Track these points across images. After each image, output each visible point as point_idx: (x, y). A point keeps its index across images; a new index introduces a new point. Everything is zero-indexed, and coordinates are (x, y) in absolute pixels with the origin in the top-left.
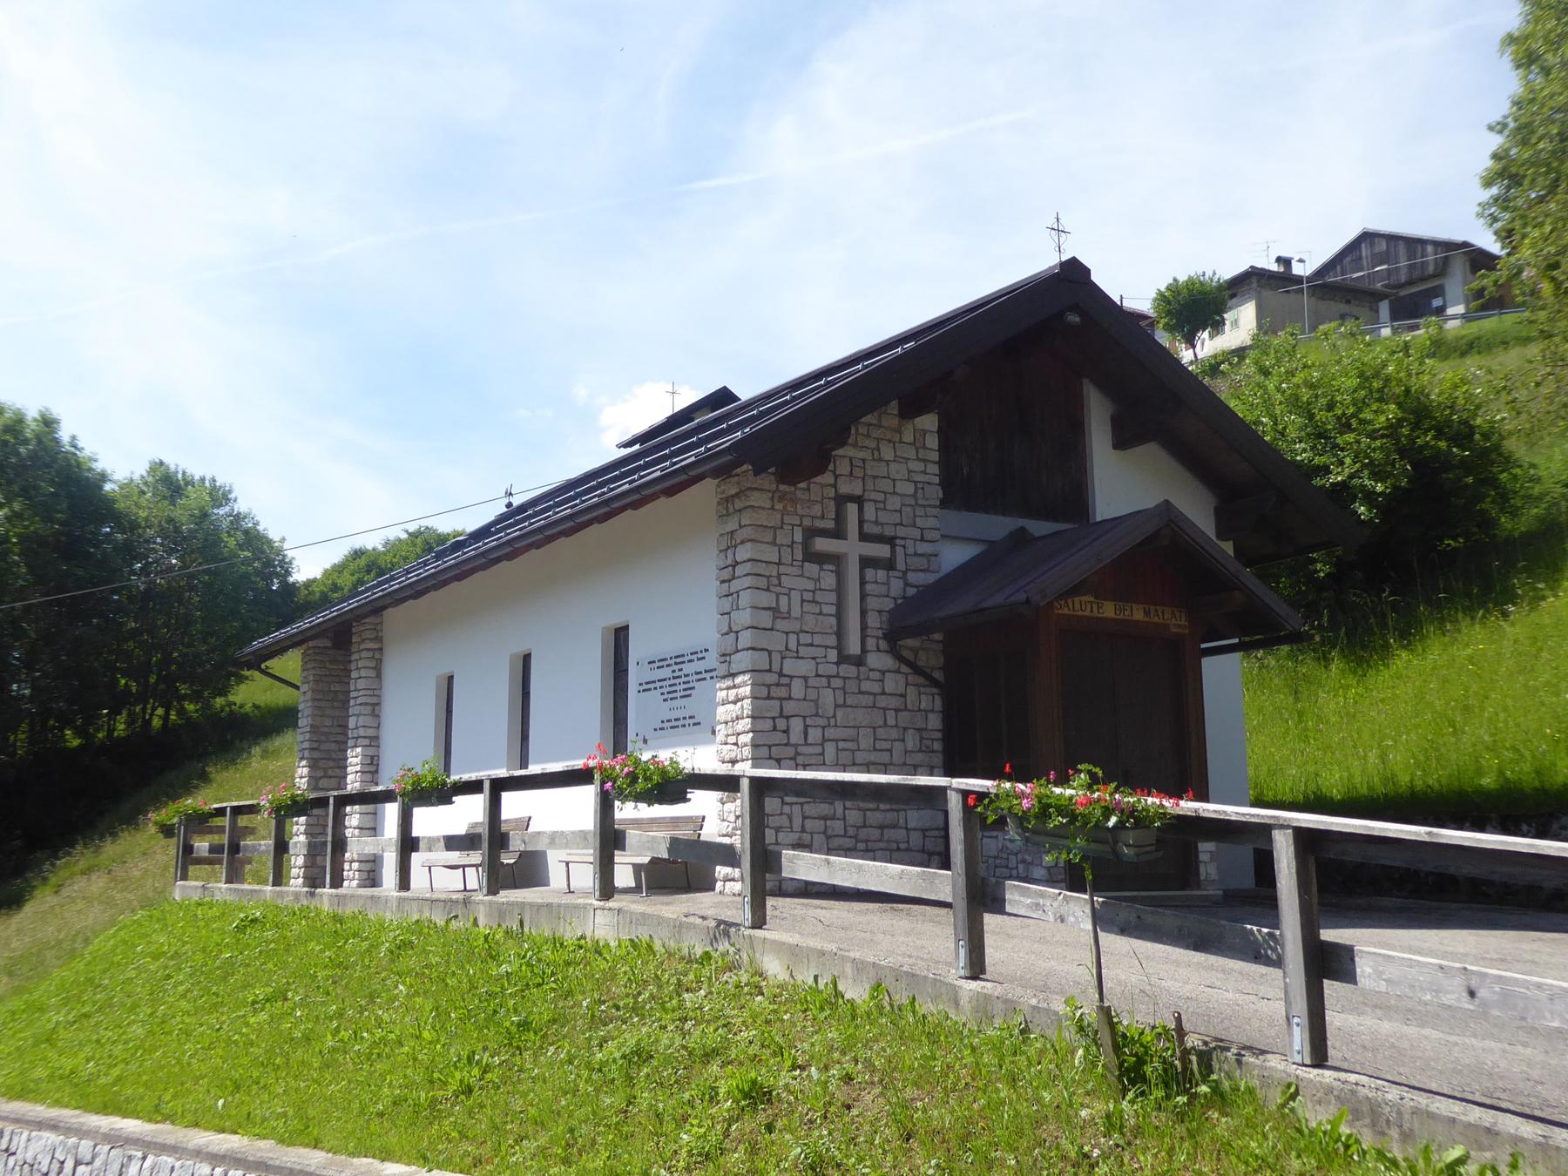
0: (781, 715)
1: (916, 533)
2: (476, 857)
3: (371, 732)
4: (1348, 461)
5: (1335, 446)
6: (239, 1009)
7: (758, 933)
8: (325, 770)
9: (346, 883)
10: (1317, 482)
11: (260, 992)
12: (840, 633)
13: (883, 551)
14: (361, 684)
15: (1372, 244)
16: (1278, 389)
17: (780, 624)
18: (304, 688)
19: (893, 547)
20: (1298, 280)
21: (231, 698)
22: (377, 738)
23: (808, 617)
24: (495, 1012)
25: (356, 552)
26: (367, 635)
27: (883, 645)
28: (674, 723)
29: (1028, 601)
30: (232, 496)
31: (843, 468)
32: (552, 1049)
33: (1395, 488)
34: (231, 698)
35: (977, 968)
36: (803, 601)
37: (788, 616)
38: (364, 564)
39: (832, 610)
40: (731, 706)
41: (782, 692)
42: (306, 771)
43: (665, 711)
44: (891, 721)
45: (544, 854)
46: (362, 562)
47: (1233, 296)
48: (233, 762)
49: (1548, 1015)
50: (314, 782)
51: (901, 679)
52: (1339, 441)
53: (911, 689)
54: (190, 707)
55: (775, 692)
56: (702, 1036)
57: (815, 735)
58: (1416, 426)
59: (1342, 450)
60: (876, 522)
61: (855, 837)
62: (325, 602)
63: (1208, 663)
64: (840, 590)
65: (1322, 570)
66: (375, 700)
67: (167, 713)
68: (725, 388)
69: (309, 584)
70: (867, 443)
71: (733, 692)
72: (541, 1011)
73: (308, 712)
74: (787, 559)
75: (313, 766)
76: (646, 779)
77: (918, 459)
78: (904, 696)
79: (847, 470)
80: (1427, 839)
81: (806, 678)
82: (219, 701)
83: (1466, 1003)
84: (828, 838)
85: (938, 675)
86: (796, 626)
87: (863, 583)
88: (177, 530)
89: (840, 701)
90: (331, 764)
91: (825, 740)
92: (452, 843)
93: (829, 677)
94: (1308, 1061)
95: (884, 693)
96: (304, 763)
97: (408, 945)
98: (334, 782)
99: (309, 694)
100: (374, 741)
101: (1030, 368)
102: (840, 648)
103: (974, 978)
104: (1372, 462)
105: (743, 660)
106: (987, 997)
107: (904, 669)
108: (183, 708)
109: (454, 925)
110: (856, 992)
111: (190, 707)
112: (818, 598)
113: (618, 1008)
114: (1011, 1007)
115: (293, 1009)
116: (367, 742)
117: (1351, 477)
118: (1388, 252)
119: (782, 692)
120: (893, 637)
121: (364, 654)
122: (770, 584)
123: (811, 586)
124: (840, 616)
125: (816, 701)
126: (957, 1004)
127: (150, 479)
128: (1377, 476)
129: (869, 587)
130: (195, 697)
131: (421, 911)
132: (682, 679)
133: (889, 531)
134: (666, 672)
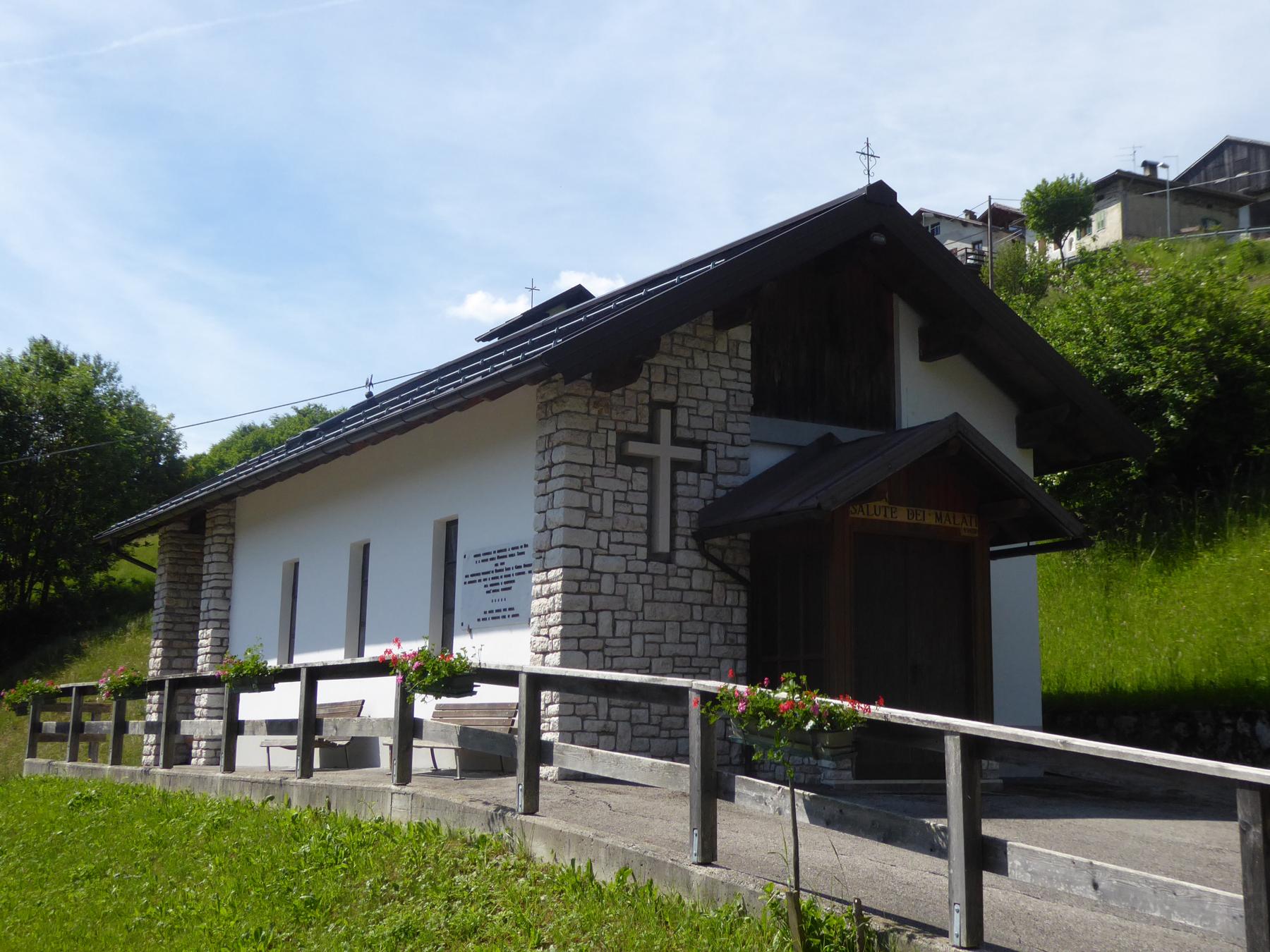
0: (591, 610)
1: (727, 438)
2: (292, 739)
3: (221, 615)
4: (1159, 371)
5: (1149, 357)
6: (60, 884)
7: (530, 819)
8: (179, 650)
9: (193, 761)
10: (1130, 391)
11: (82, 868)
12: (650, 532)
13: (693, 454)
14: (213, 568)
15: (1234, 153)
16: (1098, 301)
17: (592, 523)
18: (161, 571)
19: (704, 451)
20: (1162, 184)
21: (111, 573)
22: (227, 620)
23: (619, 517)
24: (289, 890)
25: (245, 429)
26: (219, 521)
27: (692, 543)
28: (495, 614)
29: (819, 506)
30: (117, 375)
31: (658, 376)
32: (332, 926)
33: (1201, 397)
34: (111, 573)
35: (708, 856)
36: (615, 501)
37: (600, 515)
38: (251, 440)
39: (644, 510)
40: (543, 600)
41: (593, 587)
42: (160, 651)
43: (488, 602)
44: (697, 616)
45: (376, 739)
46: (250, 439)
47: (1100, 198)
48: (108, 637)
49: (1152, 906)
50: (167, 666)
51: (708, 576)
52: (1152, 352)
53: (717, 586)
54: (69, 582)
55: (586, 587)
56: (467, 914)
57: (622, 628)
58: (1225, 340)
59: (1155, 360)
60: (689, 428)
61: (659, 725)
62: (211, 475)
63: (997, 566)
64: (652, 492)
65: (1135, 472)
66: (225, 584)
67: (46, 587)
68: (580, 286)
69: (196, 459)
70: (682, 352)
71: (546, 586)
72: (329, 891)
73: (163, 594)
74: (600, 460)
75: (167, 646)
76: (435, 673)
77: (731, 368)
78: (711, 592)
79: (661, 378)
80: (1061, 748)
81: (615, 575)
82: (98, 576)
83: (1091, 895)
84: (632, 725)
85: (745, 573)
86: (607, 524)
87: (674, 484)
88: (59, 408)
89: (648, 596)
90: (185, 644)
91: (632, 633)
92: (275, 727)
93: (638, 574)
94: (964, 944)
95: (691, 589)
96: (158, 642)
97: (224, 824)
98: (187, 662)
99: (165, 577)
100: (224, 624)
101: (845, 281)
102: (650, 545)
103: (705, 863)
104: (1181, 374)
105: (556, 555)
106: (714, 882)
107: (711, 566)
108: (63, 584)
109: (272, 805)
110: (606, 876)
111: (69, 582)
112: (630, 499)
113: (397, 888)
114: (732, 890)
115: (110, 886)
116: (217, 624)
117: (1163, 386)
118: (1248, 160)
119: (593, 587)
120: (701, 537)
121: (216, 539)
122: (584, 485)
123: (623, 487)
124: (651, 516)
125: (625, 597)
126: (689, 887)
127: (33, 357)
128: (1187, 386)
129: (680, 489)
130: (76, 572)
131: (242, 792)
132: (503, 573)
133: (701, 436)
134: (489, 566)
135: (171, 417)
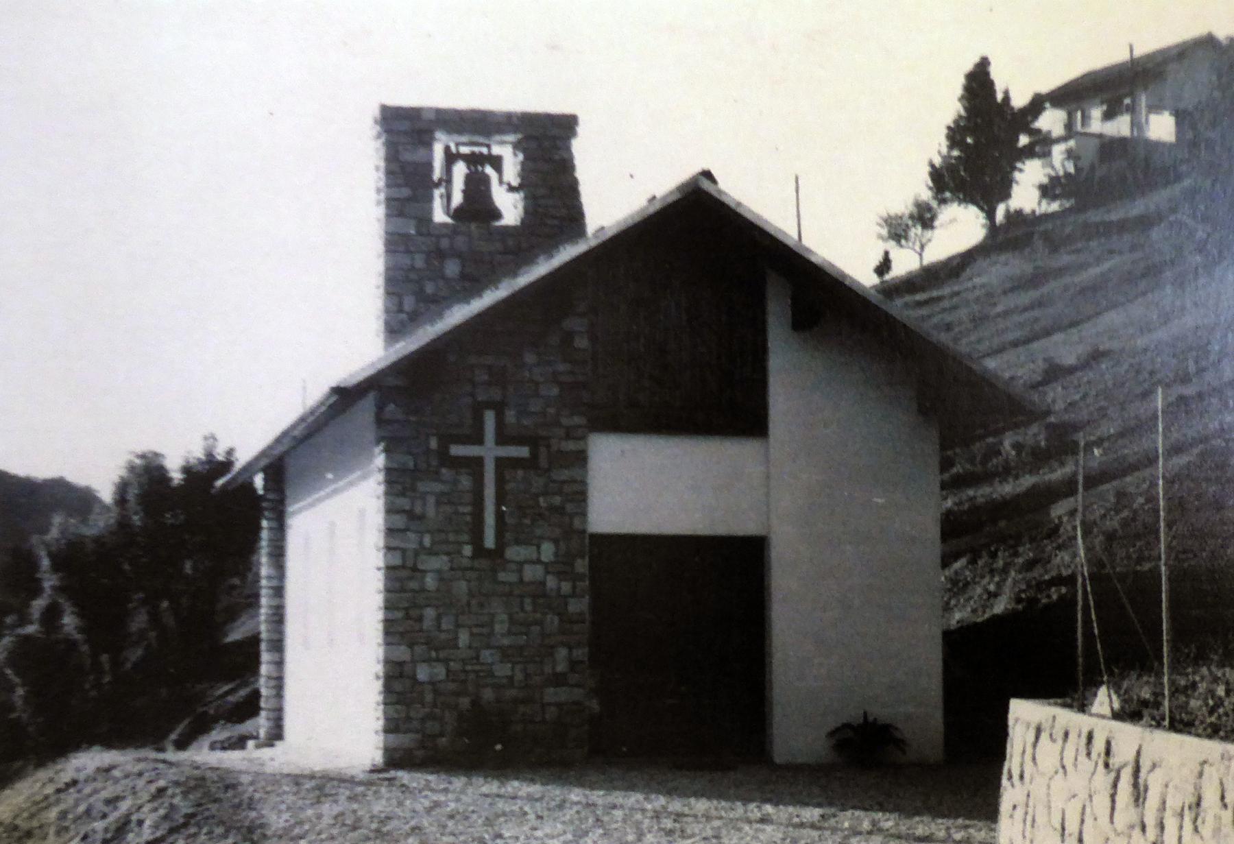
135: (379, 569)
